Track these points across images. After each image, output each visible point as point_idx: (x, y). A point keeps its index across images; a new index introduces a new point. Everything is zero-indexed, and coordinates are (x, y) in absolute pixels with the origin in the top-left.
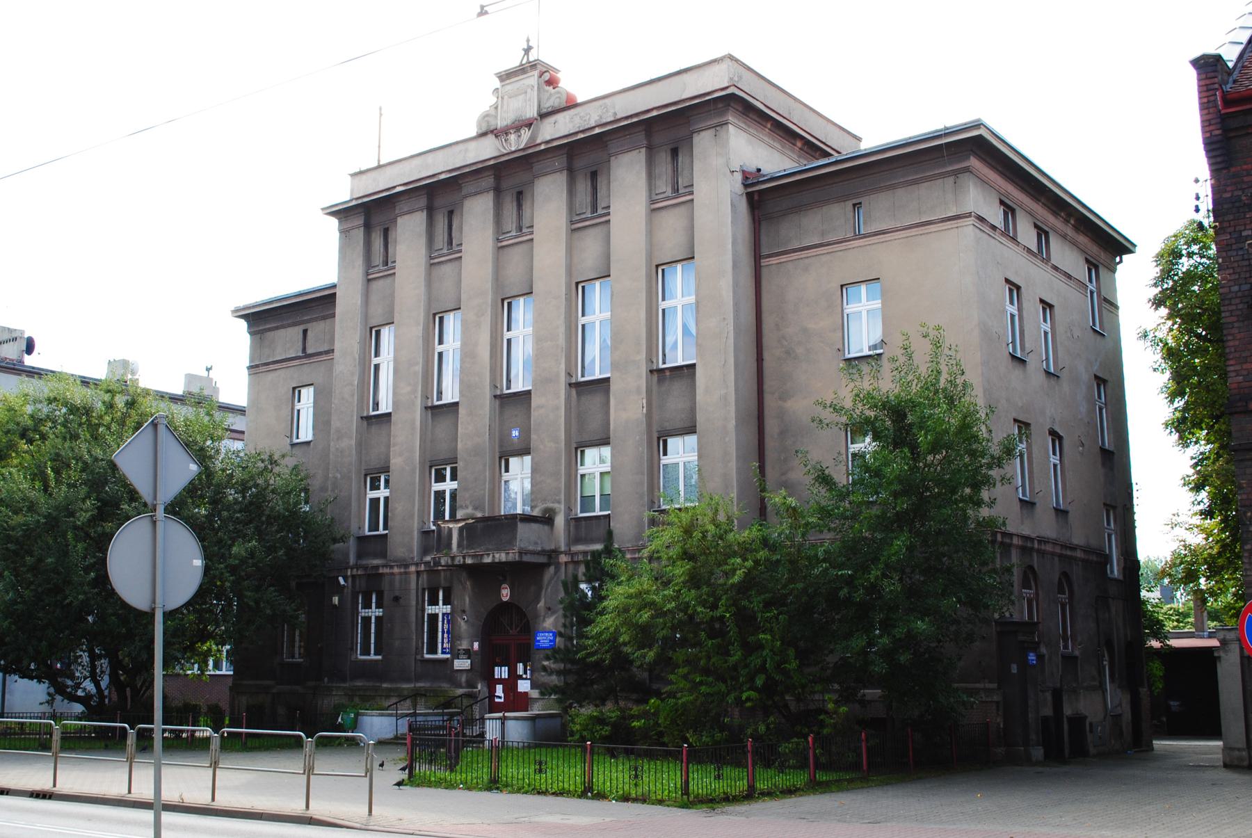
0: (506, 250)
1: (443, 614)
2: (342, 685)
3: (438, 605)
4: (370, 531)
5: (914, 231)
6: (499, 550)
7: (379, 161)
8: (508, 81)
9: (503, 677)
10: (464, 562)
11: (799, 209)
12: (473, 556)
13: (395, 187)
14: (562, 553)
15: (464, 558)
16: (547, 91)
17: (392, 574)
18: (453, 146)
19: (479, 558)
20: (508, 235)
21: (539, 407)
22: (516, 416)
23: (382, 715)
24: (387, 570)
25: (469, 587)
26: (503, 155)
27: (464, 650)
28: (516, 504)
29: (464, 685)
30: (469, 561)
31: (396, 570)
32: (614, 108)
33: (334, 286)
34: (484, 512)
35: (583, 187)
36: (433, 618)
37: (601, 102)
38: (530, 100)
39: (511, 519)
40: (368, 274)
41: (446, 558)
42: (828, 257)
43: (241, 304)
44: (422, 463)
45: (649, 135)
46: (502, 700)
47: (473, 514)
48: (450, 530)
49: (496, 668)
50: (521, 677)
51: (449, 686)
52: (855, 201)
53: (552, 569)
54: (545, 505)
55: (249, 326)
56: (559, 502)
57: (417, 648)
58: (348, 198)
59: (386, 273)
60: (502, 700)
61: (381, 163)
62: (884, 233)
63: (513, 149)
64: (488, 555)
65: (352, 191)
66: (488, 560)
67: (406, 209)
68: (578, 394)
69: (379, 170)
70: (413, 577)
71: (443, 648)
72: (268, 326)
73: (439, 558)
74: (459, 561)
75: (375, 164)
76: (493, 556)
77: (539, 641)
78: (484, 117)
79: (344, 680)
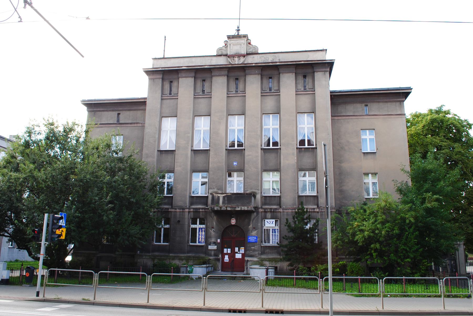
0: (230, 98)
1: (199, 228)
2: (148, 254)
3: (197, 224)
4: (167, 194)
6: (244, 206)
7: (164, 56)
8: (232, 39)
9: (228, 252)
10: (227, 209)
11: (345, 103)
12: (231, 207)
13: (253, 64)
14: (260, 208)
15: (226, 207)
16: (249, 46)
17: (176, 212)
18: (205, 57)
19: (234, 208)
20: (232, 93)
21: (249, 155)
22: (235, 157)
23: (200, 267)
24: (172, 210)
25: (215, 219)
26: (236, 64)
27: (213, 242)
28: (369, 188)
29: (213, 255)
30: (229, 209)
31: (178, 210)
32: (279, 57)
33: (146, 98)
34: (223, 191)
35: (167, 86)
36: (194, 230)
37: (273, 54)
38: (243, 48)
39: (249, 195)
40: (162, 97)
41: (217, 207)
42: (356, 120)
43: (87, 99)
44: (191, 170)
45: (195, 73)
46: (228, 261)
47: (217, 192)
48: (219, 197)
49: (225, 249)
50: (237, 253)
51: (204, 255)
52: (365, 104)
53: (255, 214)
54: (252, 191)
55: (87, 109)
56: (258, 190)
57: (188, 241)
58: (151, 67)
59: (171, 98)
60: (228, 261)
61: (165, 57)
63: (236, 63)
64: (239, 207)
65: (153, 65)
66: (239, 209)
67: (184, 76)
68: (194, 153)
69: (163, 60)
70: (187, 214)
71: (199, 241)
72: (98, 110)
73: (214, 207)
74: (224, 208)
75: (163, 57)
76: (241, 208)
77: (250, 240)
78: (220, 50)
79: (149, 252)
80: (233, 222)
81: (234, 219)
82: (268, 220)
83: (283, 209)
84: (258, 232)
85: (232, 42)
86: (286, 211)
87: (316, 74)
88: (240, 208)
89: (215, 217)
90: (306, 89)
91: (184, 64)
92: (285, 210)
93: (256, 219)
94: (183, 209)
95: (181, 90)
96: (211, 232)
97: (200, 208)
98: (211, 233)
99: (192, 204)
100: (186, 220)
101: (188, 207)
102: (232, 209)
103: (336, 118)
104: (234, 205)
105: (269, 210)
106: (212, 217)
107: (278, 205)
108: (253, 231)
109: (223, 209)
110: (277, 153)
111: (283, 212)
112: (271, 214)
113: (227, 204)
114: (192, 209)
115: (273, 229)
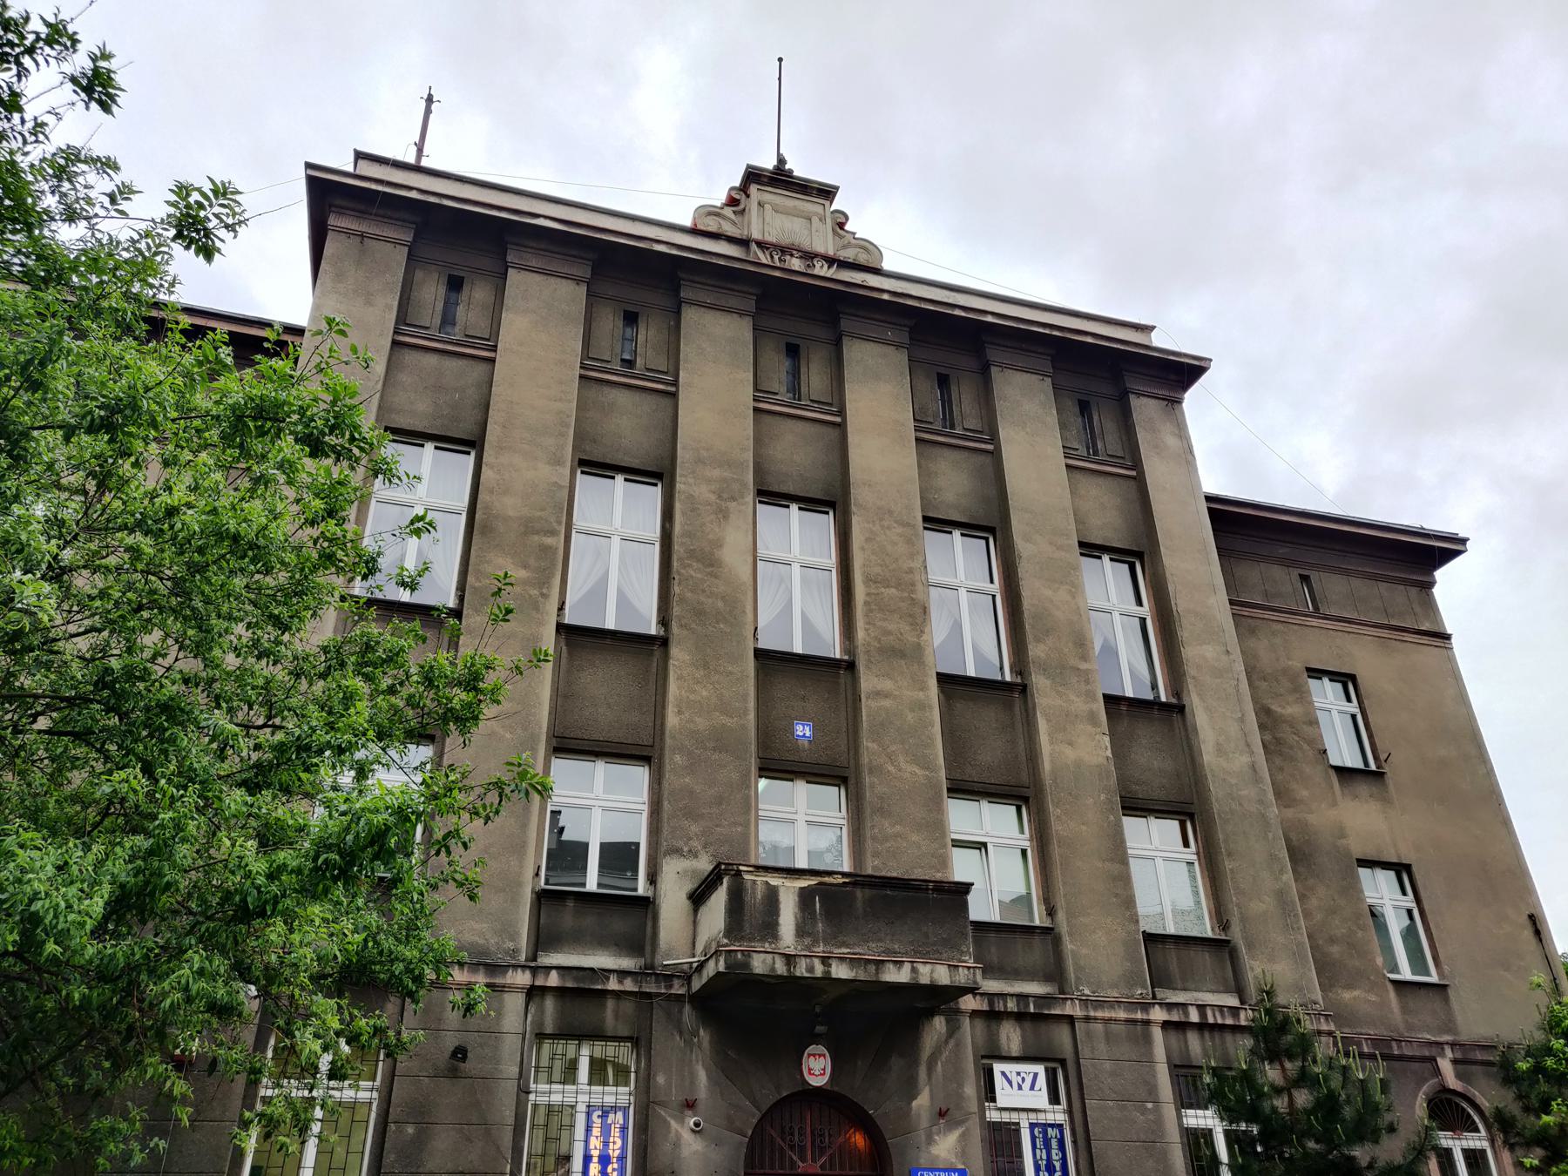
5: (1425, 640)
12: (853, 962)
21: (879, 694)
30: (841, 972)
33: (298, 331)
39: (949, 891)
48: (772, 895)
62: (1349, 622)
66: (900, 975)
70: (515, 1002)
76: (914, 970)
80: (817, 1068)
81: (821, 1049)
82: (1011, 1068)
83: (1085, 1002)
84: (963, 1136)
85: (767, 197)
86: (1099, 1014)
87: (690, 315)
88: (907, 967)
89: (704, 1035)
90: (1096, 453)
91: (548, 217)
92: (1095, 1009)
93: (946, 1054)
94: (493, 968)
95: (514, 326)
96: (678, 1137)
97: (606, 973)
98: (677, 1144)
99: (542, 939)
100: (510, 1046)
101: (523, 957)
102: (862, 976)
103: (1246, 611)
104: (869, 951)
105: (1012, 1005)
106: (681, 1033)
107: (1047, 978)
108: (939, 1133)
109: (801, 970)
110: (1009, 706)
111: (1087, 1019)
112: (1022, 1029)
113: (826, 942)
114: (554, 973)
115: (1032, 1126)
